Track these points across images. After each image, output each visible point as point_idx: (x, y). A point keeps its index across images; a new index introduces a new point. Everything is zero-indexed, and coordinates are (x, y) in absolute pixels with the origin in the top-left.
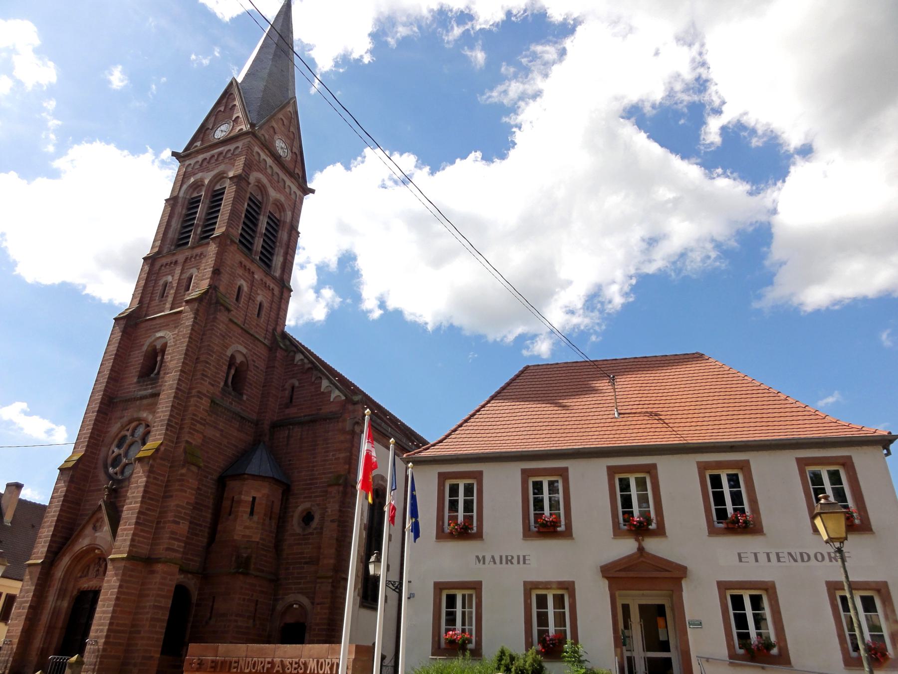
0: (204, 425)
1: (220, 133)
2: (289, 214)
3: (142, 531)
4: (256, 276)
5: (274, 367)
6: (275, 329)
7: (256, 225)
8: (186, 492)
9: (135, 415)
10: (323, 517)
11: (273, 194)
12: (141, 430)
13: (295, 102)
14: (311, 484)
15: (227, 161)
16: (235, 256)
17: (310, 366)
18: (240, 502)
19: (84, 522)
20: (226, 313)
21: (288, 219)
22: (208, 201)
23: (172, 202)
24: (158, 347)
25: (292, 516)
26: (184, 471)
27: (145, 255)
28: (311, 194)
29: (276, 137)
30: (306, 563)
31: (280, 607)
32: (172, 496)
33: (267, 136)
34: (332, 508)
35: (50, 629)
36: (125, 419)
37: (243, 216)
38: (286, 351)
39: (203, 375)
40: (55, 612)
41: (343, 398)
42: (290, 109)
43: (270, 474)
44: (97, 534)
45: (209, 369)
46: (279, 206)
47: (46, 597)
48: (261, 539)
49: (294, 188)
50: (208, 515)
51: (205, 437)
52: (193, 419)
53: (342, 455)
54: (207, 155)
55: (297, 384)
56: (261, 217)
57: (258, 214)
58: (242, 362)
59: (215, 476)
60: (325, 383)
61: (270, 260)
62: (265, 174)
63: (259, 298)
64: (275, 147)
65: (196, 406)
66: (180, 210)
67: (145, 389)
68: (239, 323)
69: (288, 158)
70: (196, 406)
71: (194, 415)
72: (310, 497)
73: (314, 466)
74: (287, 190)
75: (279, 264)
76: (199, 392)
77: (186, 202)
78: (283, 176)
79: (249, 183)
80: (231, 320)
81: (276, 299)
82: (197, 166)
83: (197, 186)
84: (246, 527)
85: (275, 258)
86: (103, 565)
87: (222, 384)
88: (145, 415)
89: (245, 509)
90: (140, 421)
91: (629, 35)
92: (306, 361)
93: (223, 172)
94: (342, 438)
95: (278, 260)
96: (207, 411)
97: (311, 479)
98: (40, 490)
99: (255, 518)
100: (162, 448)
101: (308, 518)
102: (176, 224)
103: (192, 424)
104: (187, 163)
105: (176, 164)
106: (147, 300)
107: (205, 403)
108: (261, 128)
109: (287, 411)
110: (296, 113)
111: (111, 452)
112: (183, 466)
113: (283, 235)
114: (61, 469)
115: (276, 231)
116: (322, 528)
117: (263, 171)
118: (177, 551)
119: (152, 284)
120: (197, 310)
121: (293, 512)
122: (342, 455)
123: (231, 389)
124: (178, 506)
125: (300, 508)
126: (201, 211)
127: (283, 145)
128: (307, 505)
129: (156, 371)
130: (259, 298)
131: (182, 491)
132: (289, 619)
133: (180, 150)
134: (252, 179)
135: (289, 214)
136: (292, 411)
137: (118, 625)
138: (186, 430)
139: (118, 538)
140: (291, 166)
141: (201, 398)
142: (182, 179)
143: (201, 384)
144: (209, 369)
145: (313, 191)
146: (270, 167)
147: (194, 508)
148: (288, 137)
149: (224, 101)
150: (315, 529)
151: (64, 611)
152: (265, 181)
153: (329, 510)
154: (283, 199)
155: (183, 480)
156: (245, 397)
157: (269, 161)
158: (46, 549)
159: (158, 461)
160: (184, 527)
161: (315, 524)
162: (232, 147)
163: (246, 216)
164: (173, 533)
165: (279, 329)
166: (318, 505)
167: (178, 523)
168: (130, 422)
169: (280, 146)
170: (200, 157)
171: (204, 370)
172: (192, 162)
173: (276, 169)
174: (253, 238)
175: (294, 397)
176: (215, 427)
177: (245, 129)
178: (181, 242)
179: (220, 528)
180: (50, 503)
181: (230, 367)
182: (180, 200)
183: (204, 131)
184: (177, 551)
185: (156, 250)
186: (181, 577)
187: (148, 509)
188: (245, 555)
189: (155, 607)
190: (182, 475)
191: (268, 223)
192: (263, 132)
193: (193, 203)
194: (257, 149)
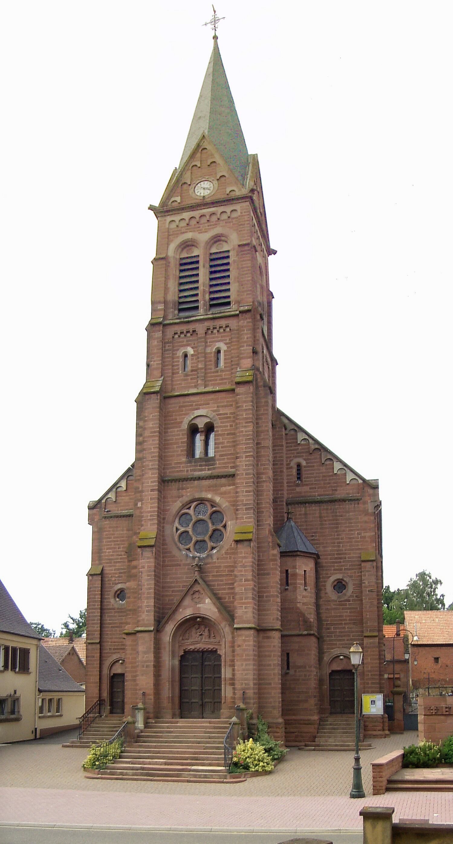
9: (197, 496)
14: (340, 558)
17: (317, 446)
22: (207, 266)
25: (325, 586)
31: (326, 658)
36: (186, 499)
44: (198, 606)
55: (304, 463)
67: (201, 470)
72: (341, 570)
73: (339, 543)
84: (304, 597)
88: (209, 496)
91: (218, 40)
99: (308, 588)
101: (340, 586)
109: (298, 489)
121: (325, 582)
125: (332, 579)
128: (340, 576)
133: (157, 204)
136: (303, 490)
142: (164, 237)
145: (275, 252)
166: (351, 577)
168: (192, 501)
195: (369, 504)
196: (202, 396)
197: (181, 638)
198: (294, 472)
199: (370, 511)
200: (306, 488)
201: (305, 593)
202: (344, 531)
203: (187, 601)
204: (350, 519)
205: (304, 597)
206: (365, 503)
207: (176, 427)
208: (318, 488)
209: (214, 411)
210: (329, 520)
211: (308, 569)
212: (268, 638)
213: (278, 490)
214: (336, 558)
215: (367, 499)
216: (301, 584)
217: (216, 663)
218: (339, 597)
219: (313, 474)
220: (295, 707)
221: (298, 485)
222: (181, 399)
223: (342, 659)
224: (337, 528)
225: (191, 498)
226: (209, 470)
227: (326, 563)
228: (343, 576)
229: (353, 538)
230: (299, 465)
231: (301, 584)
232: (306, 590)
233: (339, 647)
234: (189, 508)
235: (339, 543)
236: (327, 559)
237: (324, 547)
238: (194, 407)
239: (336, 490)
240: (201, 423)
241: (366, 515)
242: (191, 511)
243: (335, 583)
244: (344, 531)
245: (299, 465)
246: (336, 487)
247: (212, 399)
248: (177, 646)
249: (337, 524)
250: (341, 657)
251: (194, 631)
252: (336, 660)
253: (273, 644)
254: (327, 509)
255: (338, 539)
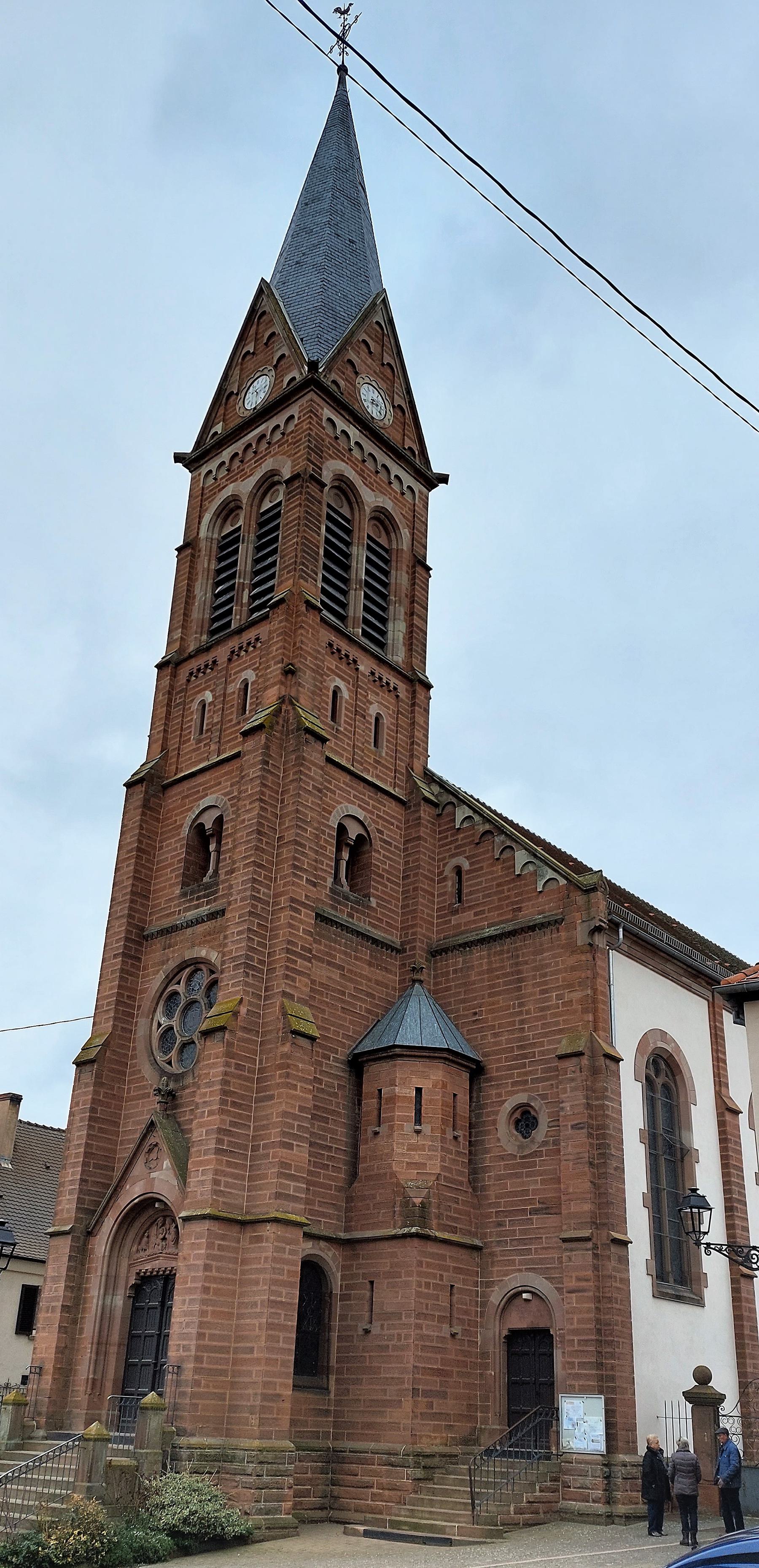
0: (309, 960)
1: (257, 393)
2: (405, 533)
3: (229, 1164)
4: (361, 668)
5: (419, 838)
6: (410, 767)
7: (347, 568)
8: (295, 1087)
10: (556, 1121)
11: (370, 498)
12: (203, 979)
13: (385, 302)
14: (524, 1056)
15: (275, 449)
16: (316, 637)
17: (487, 827)
18: (393, 1099)
19: (127, 1155)
20: (318, 746)
21: (405, 545)
23: (188, 549)
24: (208, 826)
25: (494, 1122)
26: (286, 1049)
27: (158, 660)
28: (441, 485)
29: (359, 380)
30: (535, 1211)
32: (271, 1097)
33: (342, 383)
34: (572, 1101)
35: (101, 1345)
36: (172, 965)
37: (322, 552)
38: (436, 805)
39: (295, 867)
40: (105, 1316)
41: (562, 882)
42: (379, 317)
43: (440, 1043)
44: (153, 1175)
45: (303, 854)
46: (382, 518)
47: (87, 1290)
48: (443, 1168)
49: (408, 480)
50: (341, 1133)
51: (313, 982)
52: (288, 951)
53: (577, 995)
54: (238, 447)
55: (466, 866)
56: (354, 550)
57: (348, 544)
58: (359, 836)
59: (343, 1054)
60: (521, 857)
61: (383, 633)
62: (350, 461)
63: (373, 710)
64: (358, 400)
65: (291, 926)
66: (207, 563)
67: (197, 907)
68: (343, 763)
69: (389, 420)
70: (291, 926)
71: (289, 942)
73: (522, 1022)
74: (396, 486)
75: (401, 637)
76: (293, 900)
77: (215, 546)
78: (383, 458)
79: (323, 485)
80: (329, 760)
81: (405, 707)
82: (223, 472)
83: (229, 509)
84: (412, 1148)
85: (390, 625)
86: (173, 1229)
87: (330, 880)
88: (203, 953)
89: (404, 1112)
90: (196, 965)
92: (477, 818)
93: (273, 473)
94: (571, 961)
95: (397, 630)
96: (310, 934)
97: (520, 1047)
98: (51, 1104)
99: (426, 1128)
100: (243, 1010)
101: (525, 1120)
102: (203, 592)
103: (289, 960)
104: (204, 470)
105: (184, 475)
106: (173, 744)
107: (307, 917)
108: (329, 368)
109: (454, 920)
110: (391, 321)
111: (155, 1025)
112: (284, 1040)
113: (400, 578)
114: (79, 1063)
115: (386, 573)
116: (556, 1143)
117: (345, 455)
118: (295, 1199)
119: (176, 712)
120: (267, 747)
121: (496, 1113)
122: (577, 995)
123: (346, 888)
124: (285, 1114)
125: (508, 1106)
126: (245, 554)
127: (375, 395)
128: (522, 1098)
129: (211, 871)
130: (373, 710)
131: (288, 1085)
132: (519, 1321)
134: (327, 477)
135: (405, 533)
137: (212, 1337)
138: (280, 972)
139: (192, 1180)
140: (394, 436)
141: (298, 911)
143: (294, 884)
144: (303, 854)
146: (357, 443)
147: (314, 1117)
148: (384, 378)
149: (253, 331)
150: (544, 1143)
151: (118, 1313)
152: (351, 474)
153: (567, 1105)
154: (389, 506)
155: (288, 1066)
156: (373, 902)
157: (354, 432)
158: (74, 1206)
159: (240, 1034)
160: (301, 1154)
161: (541, 1133)
162: (280, 419)
163: (327, 554)
164: (284, 1165)
165: (417, 765)
167: (290, 1146)
168: (181, 968)
169: (372, 399)
170: (226, 455)
171: (295, 859)
172: (213, 465)
173: (369, 447)
174: (344, 593)
175: (465, 891)
176: (329, 963)
177: (298, 378)
178: (220, 628)
179: (363, 1149)
180: (70, 1123)
181: (339, 850)
182: (203, 545)
183: (224, 397)
184: (295, 1199)
185: (176, 646)
186: (309, 1248)
187: (233, 1124)
188: (418, 1201)
189: (272, 1303)
190: (285, 1056)
191: (368, 560)
192: (333, 376)
193: (228, 546)
194: (327, 412)
195: (579, 928)
196: (212, 771)
197: (134, 1249)
198: (450, 886)
199: (579, 943)
200: (469, 915)
201: (414, 1140)
202: (532, 994)
203: (139, 1168)
204: (543, 967)
205: (412, 1148)
206: (573, 926)
207: (173, 836)
208: (489, 911)
209: (225, 795)
210: (505, 975)
211: (426, 1085)
212: (259, 1239)
213: (408, 927)
214: (516, 1058)
215: (577, 917)
216: (406, 1119)
217: (205, 1308)
218: (521, 1147)
219: (481, 883)
220: (379, 1420)
221: (456, 912)
222: (186, 785)
223: (526, 1300)
224: (519, 989)
225: (178, 962)
226: (208, 903)
227: (498, 1069)
228: (531, 1098)
229: (548, 1008)
230: (458, 871)
231: (406, 1119)
232: (418, 1132)
233: (520, 1270)
234: (179, 983)
235: (522, 1022)
236: (499, 1060)
237: (495, 1035)
238: (201, 794)
239: (520, 909)
240: (208, 821)
241: (573, 952)
242: (181, 988)
243: (517, 1115)
244: (532, 994)
245: (458, 871)
246: (522, 901)
247: (225, 774)
248: (125, 1263)
249: (520, 980)
250: (525, 1296)
251: (154, 1230)
252: (517, 1301)
253: (264, 1255)
254: (502, 952)
255: (521, 1013)
